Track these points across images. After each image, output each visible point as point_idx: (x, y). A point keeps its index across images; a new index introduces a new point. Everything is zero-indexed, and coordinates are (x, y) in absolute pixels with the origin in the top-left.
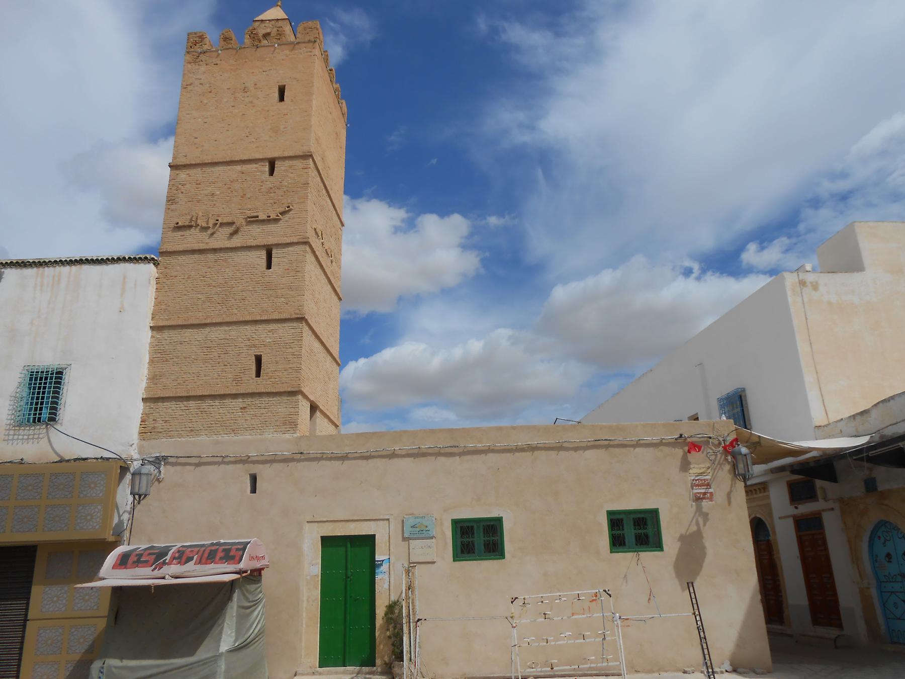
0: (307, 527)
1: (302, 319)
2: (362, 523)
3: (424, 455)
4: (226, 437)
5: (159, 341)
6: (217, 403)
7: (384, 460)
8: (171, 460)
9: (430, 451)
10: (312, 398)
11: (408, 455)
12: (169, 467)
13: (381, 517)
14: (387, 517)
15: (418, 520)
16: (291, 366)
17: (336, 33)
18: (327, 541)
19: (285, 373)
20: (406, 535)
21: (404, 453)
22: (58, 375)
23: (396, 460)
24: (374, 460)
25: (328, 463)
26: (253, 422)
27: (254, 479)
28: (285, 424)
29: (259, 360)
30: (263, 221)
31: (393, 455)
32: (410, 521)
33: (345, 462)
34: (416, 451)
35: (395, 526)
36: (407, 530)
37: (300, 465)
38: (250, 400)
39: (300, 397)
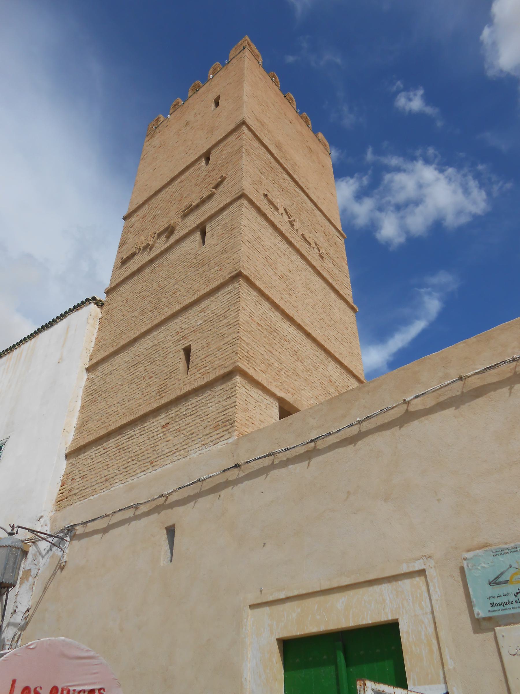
0: (251, 618)
1: (239, 275)
2: (361, 591)
3: (478, 393)
4: (143, 477)
5: (93, 379)
6: (137, 430)
7: (387, 433)
8: (80, 530)
9: (492, 377)
10: (280, 394)
11: (441, 406)
12: (75, 542)
13: (405, 568)
14: (417, 566)
15: (504, 561)
16: (226, 340)
17: (430, 294)
18: (294, 650)
19: (219, 353)
20: (481, 612)
21: (430, 402)
22: (173, 526)
23: (416, 423)
24: (369, 439)
25: (283, 471)
26: (176, 441)
27: (171, 531)
28: (216, 427)
29: (187, 351)
30: (198, 206)
31: (409, 416)
32: (484, 567)
33: (314, 461)
34: (457, 389)
35: (442, 586)
36: (481, 593)
37: (237, 490)
38: (174, 410)
39: (238, 379)
